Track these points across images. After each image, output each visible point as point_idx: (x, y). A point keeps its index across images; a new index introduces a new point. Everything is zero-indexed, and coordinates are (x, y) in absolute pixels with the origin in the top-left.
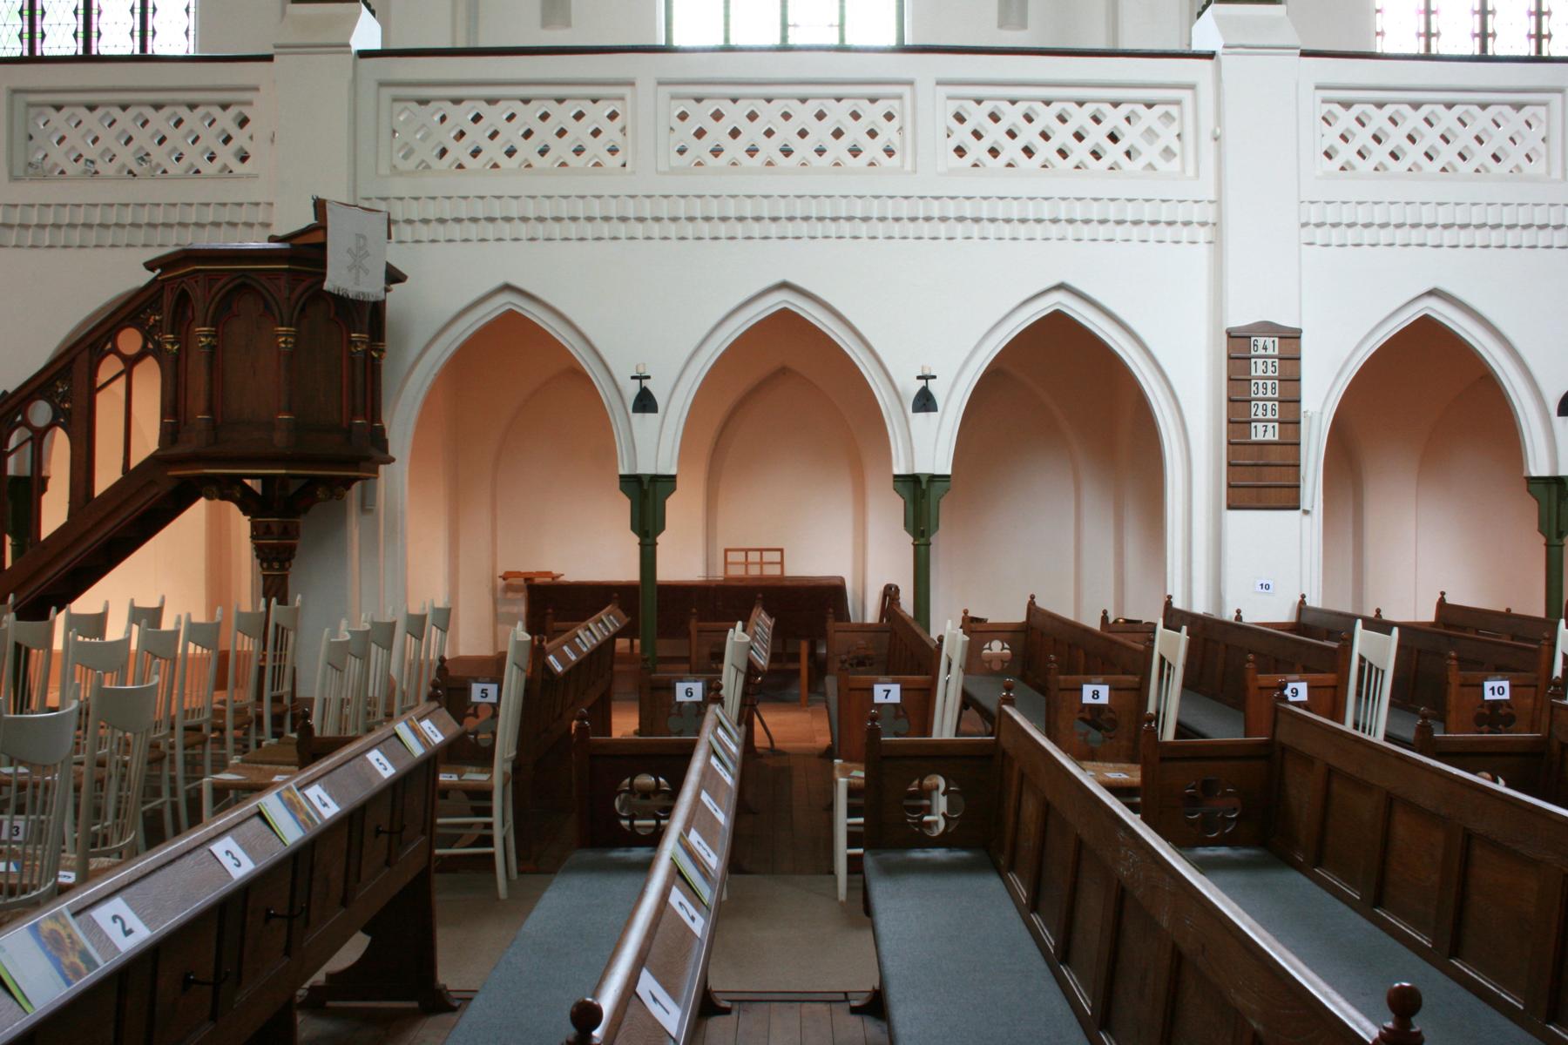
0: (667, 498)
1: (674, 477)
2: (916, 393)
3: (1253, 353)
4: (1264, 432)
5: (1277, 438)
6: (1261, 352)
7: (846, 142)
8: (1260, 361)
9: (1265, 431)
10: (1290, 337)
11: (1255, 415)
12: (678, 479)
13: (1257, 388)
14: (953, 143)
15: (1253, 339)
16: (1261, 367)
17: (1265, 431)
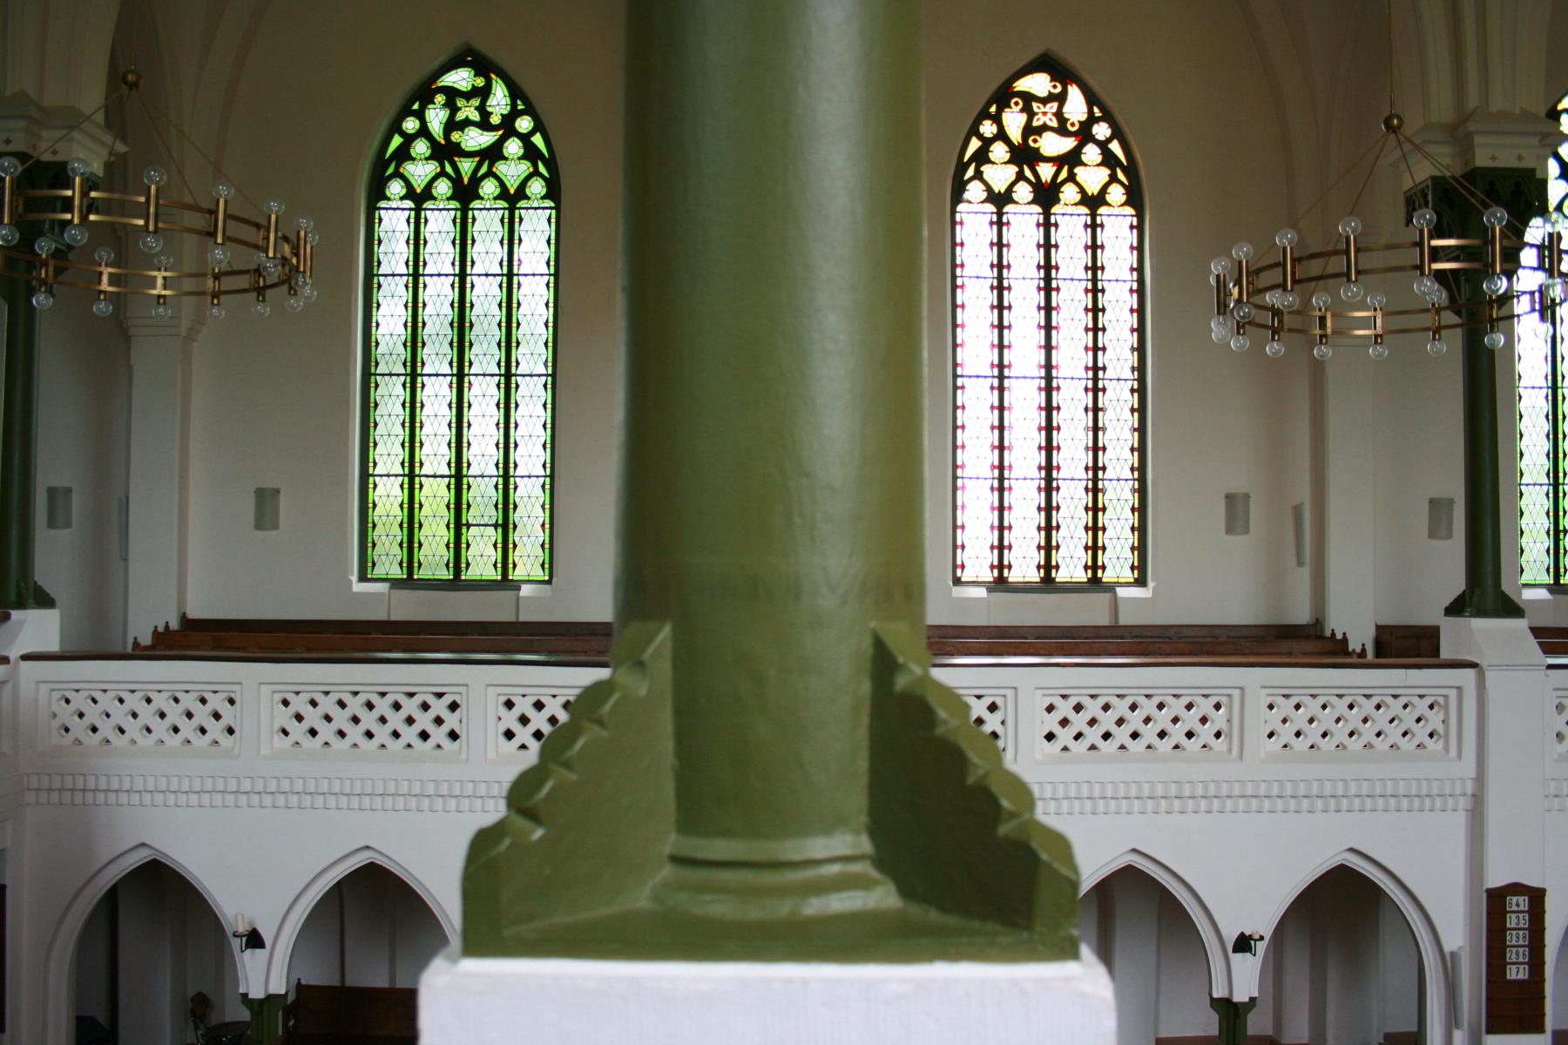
0: (1248, 1013)
2: (1236, 936)
6: (1515, 908)
7: (416, 728)
8: (1513, 916)
9: (1518, 972)
10: (1536, 897)
11: (1510, 958)
14: (502, 728)
15: (1508, 898)
16: (1514, 920)
17: (1518, 972)
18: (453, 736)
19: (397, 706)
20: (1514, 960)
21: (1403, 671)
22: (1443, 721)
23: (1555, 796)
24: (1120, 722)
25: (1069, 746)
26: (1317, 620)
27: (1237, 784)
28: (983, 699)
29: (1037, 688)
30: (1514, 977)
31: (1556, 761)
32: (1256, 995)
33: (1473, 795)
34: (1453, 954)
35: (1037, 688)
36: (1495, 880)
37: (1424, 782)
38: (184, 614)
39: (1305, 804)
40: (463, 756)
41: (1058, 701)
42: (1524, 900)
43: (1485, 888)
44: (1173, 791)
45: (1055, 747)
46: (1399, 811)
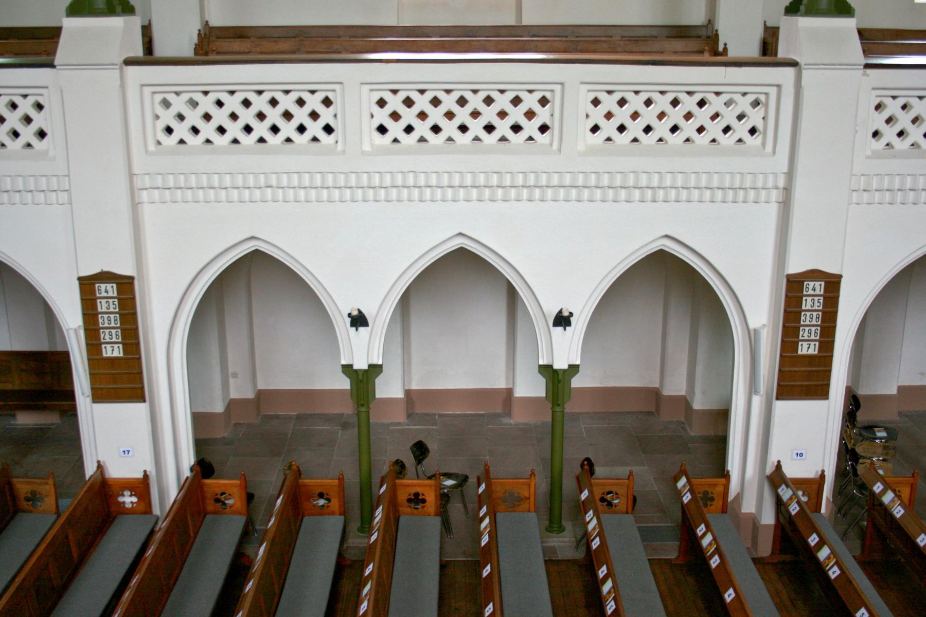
0: (572, 377)
1: (579, 365)
3: (805, 293)
4: (112, 351)
5: (122, 355)
8: (104, 301)
10: (125, 285)
12: (580, 366)
13: (103, 320)
15: (805, 283)
17: (113, 350)
18: (328, 129)
19: (301, 102)
20: (806, 338)
21: (722, 69)
22: (763, 118)
23: (865, 190)
24: (661, 116)
25: (399, 138)
26: (710, 21)
27: (704, 176)
28: (316, 94)
29: (362, 84)
30: (804, 352)
31: (868, 157)
32: (578, 363)
33: (785, 189)
34: (755, 330)
35: (362, 84)
36: (795, 267)
37: (738, 176)
38: (207, 22)
39: (623, 194)
40: (769, 148)
41: (388, 96)
42: (821, 285)
43: (786, 273)
44: (495, 180)
45: (879, 145)
46: (735, 202)
